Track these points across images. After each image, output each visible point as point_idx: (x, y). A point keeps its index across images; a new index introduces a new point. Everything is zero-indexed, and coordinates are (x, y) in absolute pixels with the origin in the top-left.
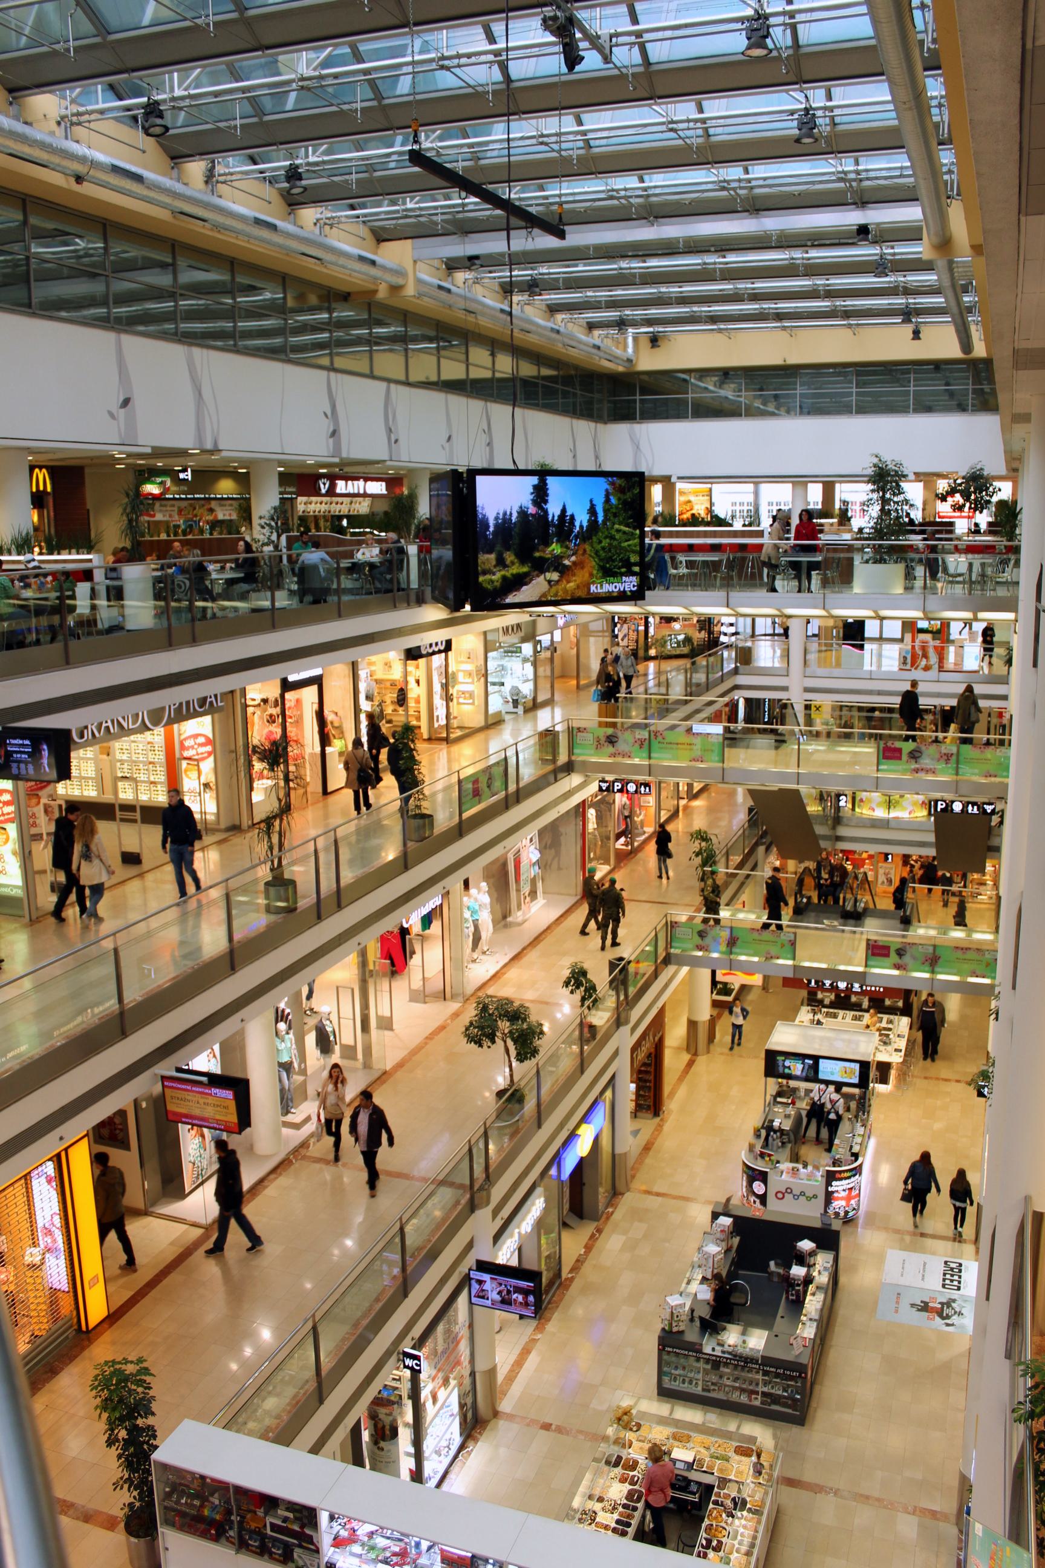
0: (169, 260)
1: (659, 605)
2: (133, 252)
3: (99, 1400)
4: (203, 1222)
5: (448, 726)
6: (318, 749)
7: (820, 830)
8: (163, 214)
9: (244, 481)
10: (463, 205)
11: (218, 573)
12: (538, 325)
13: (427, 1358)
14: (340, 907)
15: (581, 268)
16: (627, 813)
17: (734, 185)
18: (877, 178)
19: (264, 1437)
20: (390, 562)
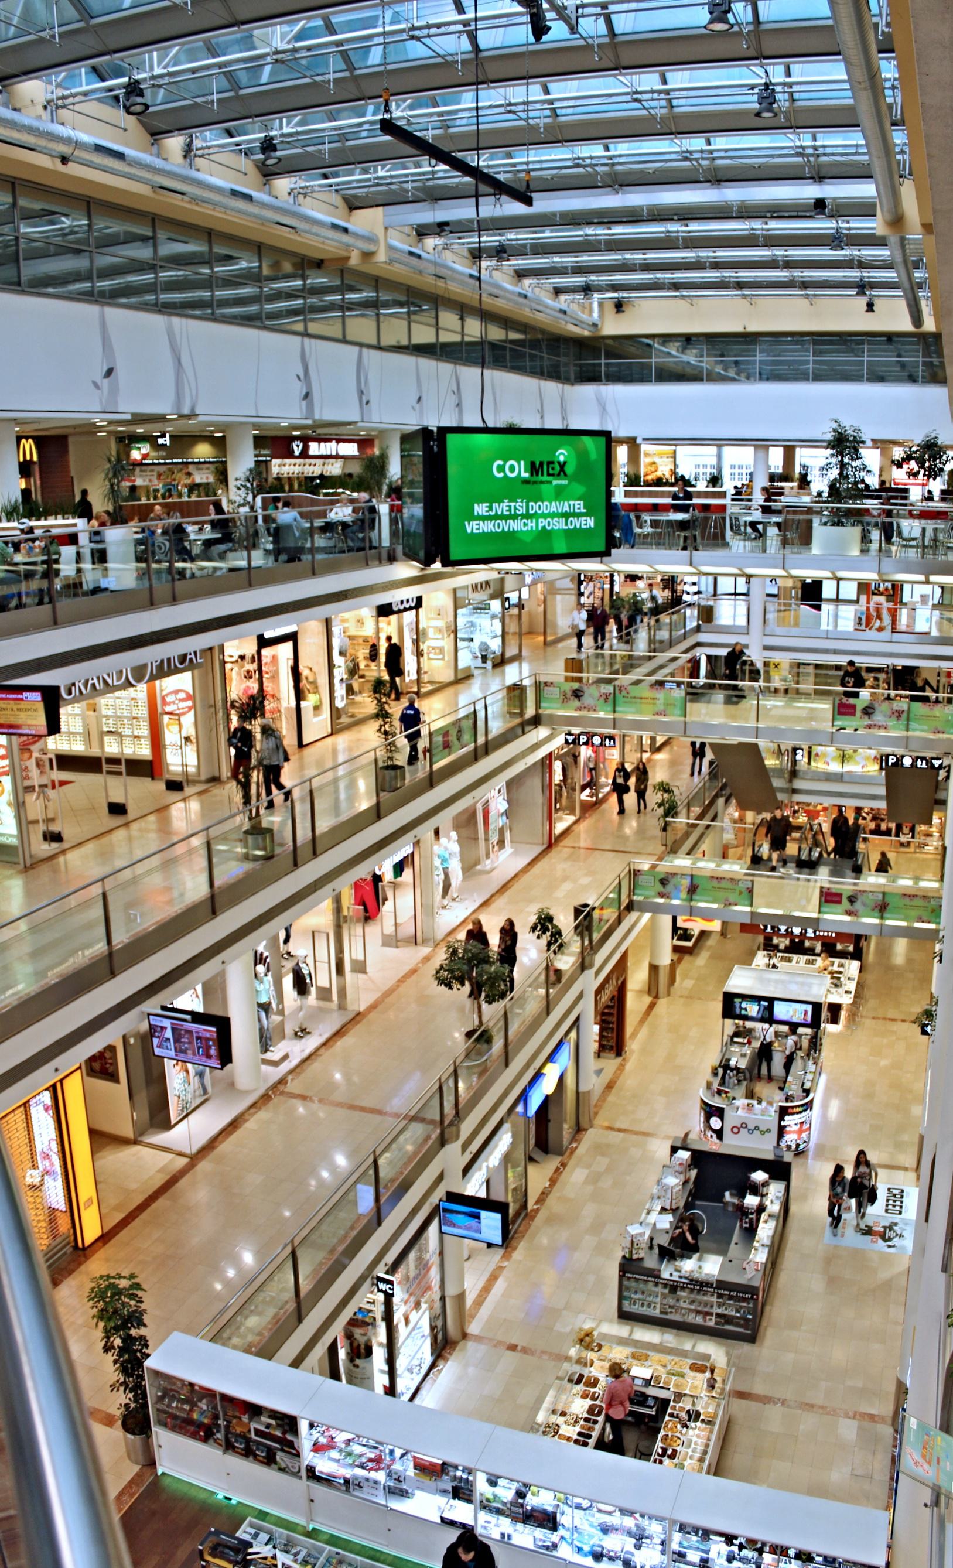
0: (150, 234)
1: (624, 562)
2: (116, 227)
3: (95, 1310)
4: (188, 1151)
5: (418, 681)
6: (293, 703)
7: (777, 783)
8: (144, 190)
9: (220, 444)
10: (433, 173)
11: (196, 534)
12: (505, 290)
13: (399, 1283)
14: (315, 854)
15: (548, 235)
16: (592, 766)
17: (696, 155)
18: (833, 154)
19: (247, 1350)
20: (362, 521)
